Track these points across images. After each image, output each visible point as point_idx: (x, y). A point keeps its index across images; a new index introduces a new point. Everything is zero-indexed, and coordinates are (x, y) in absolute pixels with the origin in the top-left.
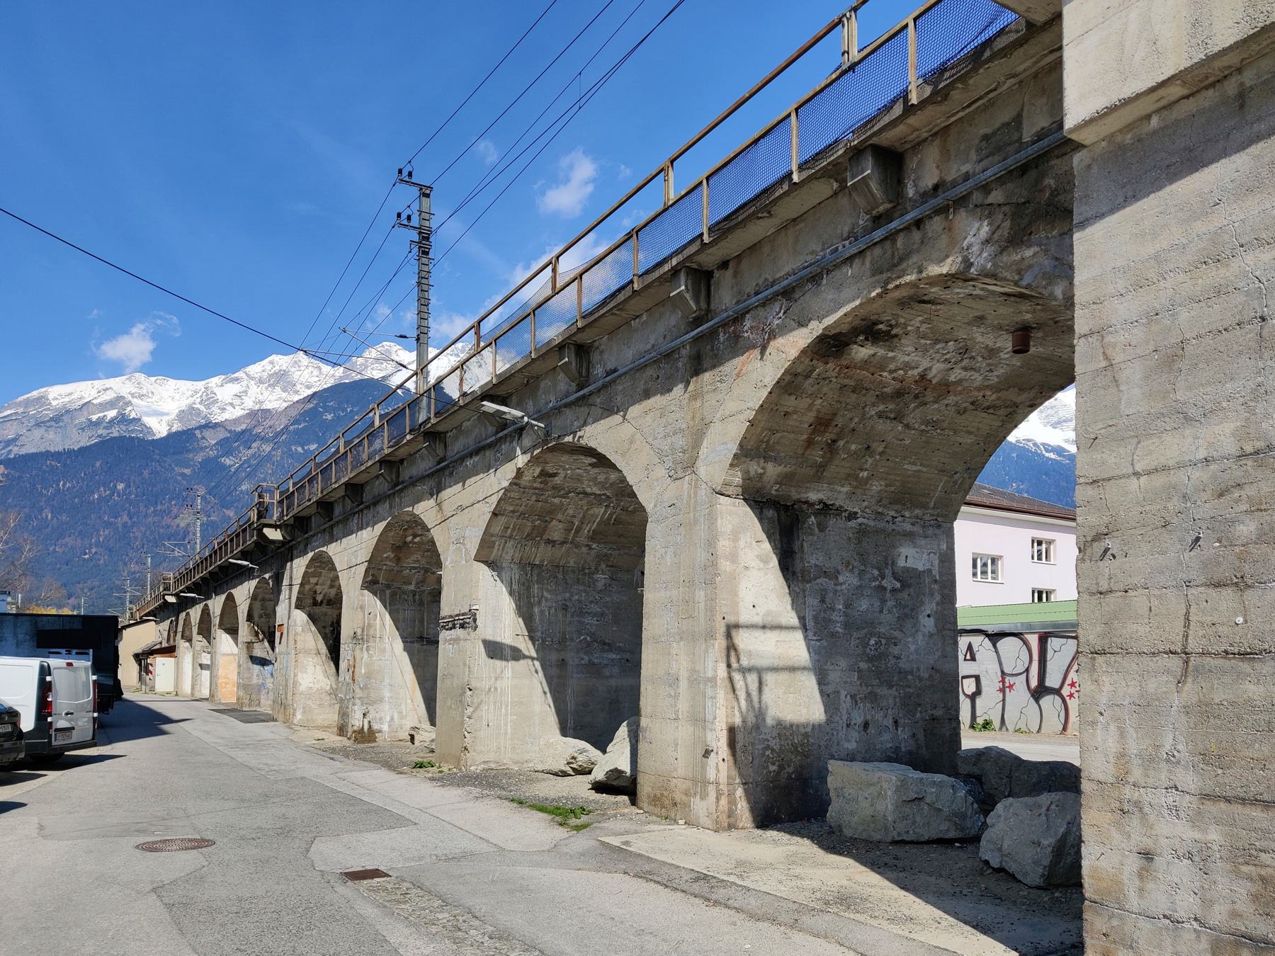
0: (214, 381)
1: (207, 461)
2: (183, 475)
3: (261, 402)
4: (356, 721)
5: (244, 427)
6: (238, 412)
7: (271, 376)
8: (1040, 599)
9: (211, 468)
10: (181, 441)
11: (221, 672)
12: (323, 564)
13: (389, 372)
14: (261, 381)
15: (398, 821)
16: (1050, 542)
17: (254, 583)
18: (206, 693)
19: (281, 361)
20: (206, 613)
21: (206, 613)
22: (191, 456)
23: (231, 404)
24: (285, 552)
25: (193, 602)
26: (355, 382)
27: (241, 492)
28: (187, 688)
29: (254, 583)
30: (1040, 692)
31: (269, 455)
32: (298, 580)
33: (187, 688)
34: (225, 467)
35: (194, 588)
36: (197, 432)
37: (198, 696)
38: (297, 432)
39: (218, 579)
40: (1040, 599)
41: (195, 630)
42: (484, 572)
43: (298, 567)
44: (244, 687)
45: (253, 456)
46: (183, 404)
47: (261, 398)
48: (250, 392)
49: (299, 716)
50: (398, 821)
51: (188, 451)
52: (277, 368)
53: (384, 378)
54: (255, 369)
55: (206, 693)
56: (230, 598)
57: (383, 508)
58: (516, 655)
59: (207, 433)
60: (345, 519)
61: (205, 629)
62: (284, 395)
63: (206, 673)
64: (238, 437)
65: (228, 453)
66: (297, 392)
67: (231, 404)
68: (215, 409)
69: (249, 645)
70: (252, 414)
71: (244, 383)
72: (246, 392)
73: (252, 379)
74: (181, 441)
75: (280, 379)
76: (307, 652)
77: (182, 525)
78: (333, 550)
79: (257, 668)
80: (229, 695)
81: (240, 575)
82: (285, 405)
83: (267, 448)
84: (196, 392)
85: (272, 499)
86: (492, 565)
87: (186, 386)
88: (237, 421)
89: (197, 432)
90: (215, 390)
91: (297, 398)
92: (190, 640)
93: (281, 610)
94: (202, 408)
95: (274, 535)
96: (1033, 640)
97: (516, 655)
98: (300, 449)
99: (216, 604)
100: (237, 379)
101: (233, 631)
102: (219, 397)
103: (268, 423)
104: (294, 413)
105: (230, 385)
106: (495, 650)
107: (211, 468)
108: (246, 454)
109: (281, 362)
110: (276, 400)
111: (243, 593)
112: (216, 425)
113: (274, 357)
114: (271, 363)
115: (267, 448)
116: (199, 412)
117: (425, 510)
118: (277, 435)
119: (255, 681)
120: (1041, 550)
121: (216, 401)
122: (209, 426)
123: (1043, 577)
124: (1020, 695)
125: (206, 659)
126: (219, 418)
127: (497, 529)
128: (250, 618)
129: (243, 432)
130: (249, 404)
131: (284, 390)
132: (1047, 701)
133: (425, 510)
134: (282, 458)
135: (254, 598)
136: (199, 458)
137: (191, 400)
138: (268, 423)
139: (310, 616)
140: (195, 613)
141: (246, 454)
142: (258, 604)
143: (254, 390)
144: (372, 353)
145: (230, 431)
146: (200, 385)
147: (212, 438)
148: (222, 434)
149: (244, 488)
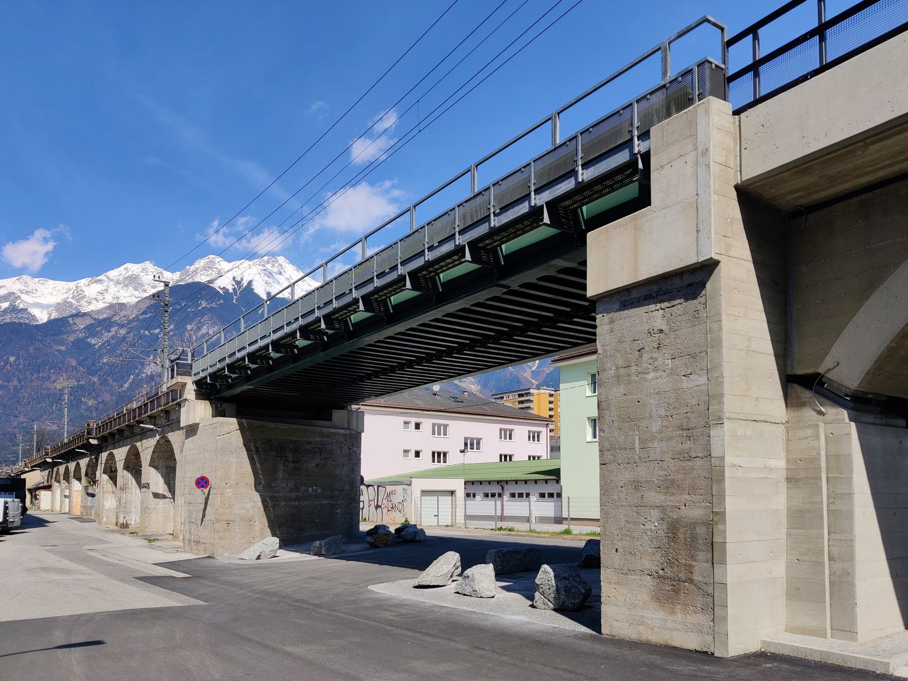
0: (83, 282)
1: (76, 342)
2: (59, 350)
3: (118, 298)
4: (121, 520)
5: (105, 316)
6: (101, 305)
7: (125, 279)
8: (505, 460)
9: (80, 346)
10: (58, 326)
11: (74, 500)
12: (111, 457)
13: (213, 277)
14: (118, 283)
15: (108, 542)
16: (511, 431)
17: (88, 459)
18: (67, 510)
19: (133, 268)
20: (67, 469)
21: (67, 469)
22: (65, 337)
23: (96, 299)
24: (96, 451)
25: (61, 464)
26: (188, 284)
27: (104, 364)
28: (58, 507)
29: (88, 459)
30: (377, 507)
31: (124, 338)
32: (104, 462)
33: (58, 507)
34: (90, 346)
35: (58, 457)
36: (70, 319)
37: (63, 511)
38: (144, 320)
39: (70, 455)
40: (505, 460)
41: (62, 478)
42: (153, 470)
43: (104, 456)
44: (84, 507)
45: (113, 337)
46: (59, 299)
47: (118, 294)
48: (110, 290)
49: (104, 520)
50: (108, 542)
51: (63, 333)
52: (130, 273)
53: (211, 281)
54: (113, 274)
55: (67, 510)
56: (78, 464)
57: (129, 440)
58: (164, 497)
59: (77, 320)
60: (119, 441)
61: (67, 478)
62: (136, 293)
63: (67, 500)
64: (101, 323)
65: (93, 335)
66: (145, 291)
67: (96, 299)
68: (83, 302)
69: (86, 488)
70: (111, 306)
71: (105, 284)
72: (106, 290)
73: (112, 281)
74: (57, 326)
75: (133, 281)
76: (108, 492)
77: (59, 387)
78: (115, 452)
79: (90, 498)
80: (77, 511)
81: (83, 455)
82: (137, 300)
83: (123, 332)
84: (69, 290)
85: (93, 425)
86: (155, 467)
87: (62, 285)
88: (99, 312)
89: (70, 319)
90: (84, 288)
91: (145, 295)
92: (59, 482)
93: (98, 473)
94: (73, 301)
95: (94, 442)
96: (376, 487)
97: (164, 497)
98: (147, 333)
99: (72, 466)
100: (100, 281)
101: (79, 479)
102: (87, 294)
103: (123, 313)
104: (143, 307)
105: (95, 285)
106: (156, 495)
107: (80, 346)
108: (107, 336)
109: (133, 269)
110: (129, 297)
111: (84, 462)
112: (84, 314)
113: (128, 265)
114: (126, 269)
115: (123, 332)
116: (71, 305)
117: (138, 444)
118: (130, 322)
119: (89, 504)
120: (508, 435)
121: (84, 297)
122: (79, 315)
123: (506, 447)
124: (373, 508)
125: (67, 493)
126: (86, 309)
127: (155, 456)
128: (86, 475)
129: (105, 320)
130: (109, 299)
131: (136, 289)
132: (379, 509)
133: (138, 444)
134: (134, 339)
135: (88, 466)
136: (72, 338)
137: (65, 296)
138: (123, 313)
139: (110, 477)
140: (62, 469)
141: (107, 336)
142: (90, 469)
143: (113, 289)
144: (202, 263)
145: (95, 319)
146: (72, 285)
147: (81, 324)
148: (88, 321)
149: (105, 360)
